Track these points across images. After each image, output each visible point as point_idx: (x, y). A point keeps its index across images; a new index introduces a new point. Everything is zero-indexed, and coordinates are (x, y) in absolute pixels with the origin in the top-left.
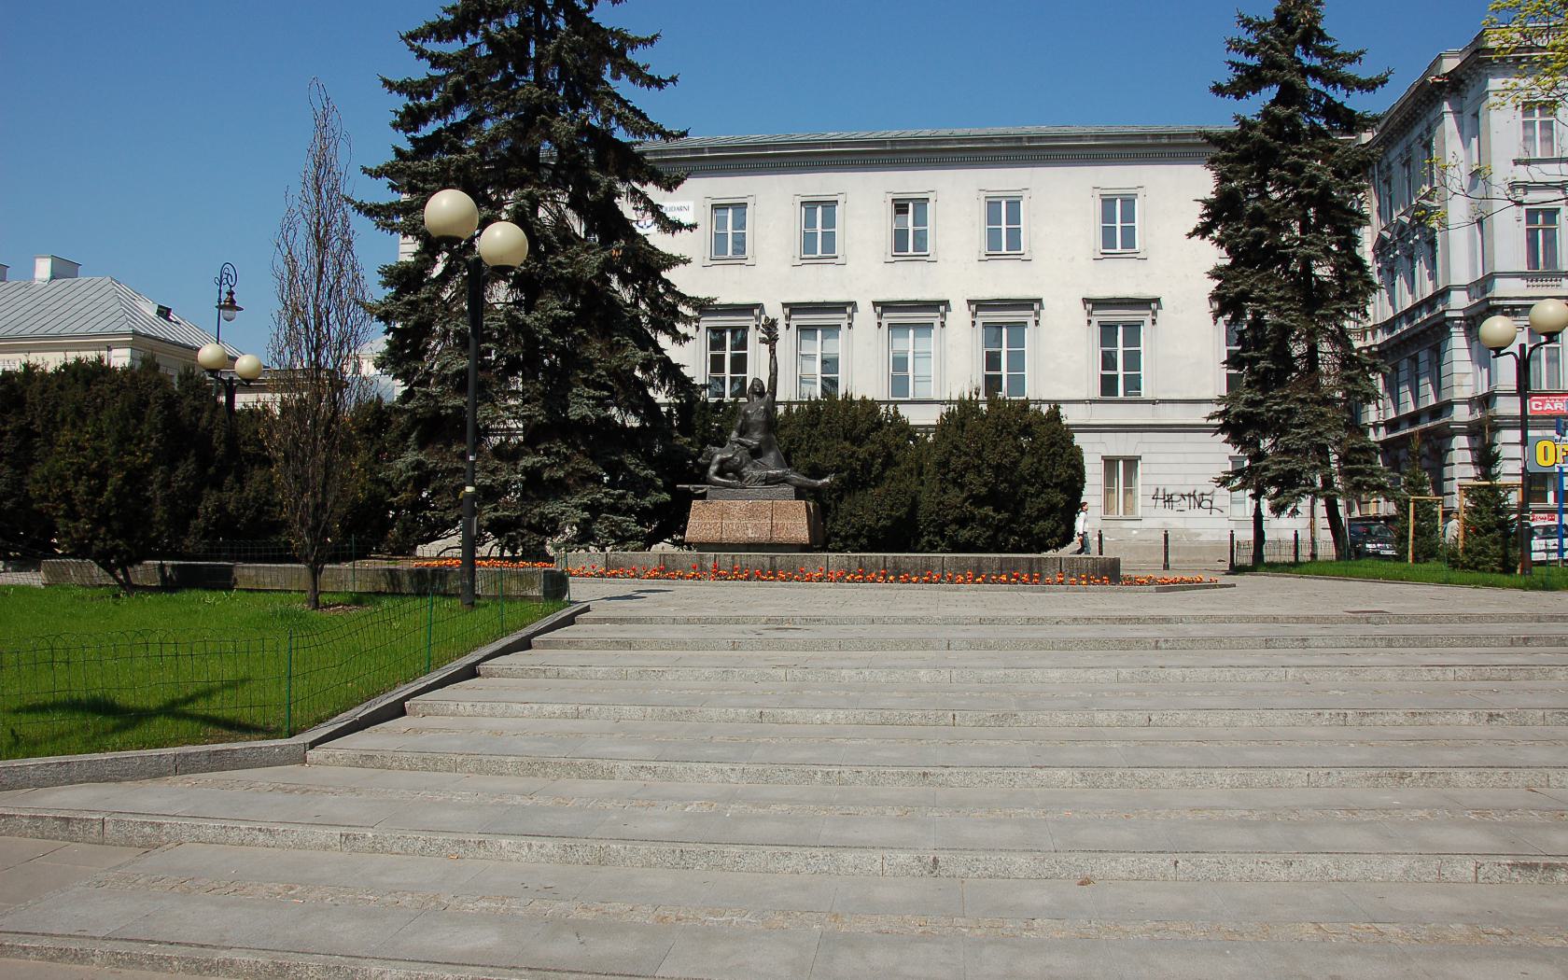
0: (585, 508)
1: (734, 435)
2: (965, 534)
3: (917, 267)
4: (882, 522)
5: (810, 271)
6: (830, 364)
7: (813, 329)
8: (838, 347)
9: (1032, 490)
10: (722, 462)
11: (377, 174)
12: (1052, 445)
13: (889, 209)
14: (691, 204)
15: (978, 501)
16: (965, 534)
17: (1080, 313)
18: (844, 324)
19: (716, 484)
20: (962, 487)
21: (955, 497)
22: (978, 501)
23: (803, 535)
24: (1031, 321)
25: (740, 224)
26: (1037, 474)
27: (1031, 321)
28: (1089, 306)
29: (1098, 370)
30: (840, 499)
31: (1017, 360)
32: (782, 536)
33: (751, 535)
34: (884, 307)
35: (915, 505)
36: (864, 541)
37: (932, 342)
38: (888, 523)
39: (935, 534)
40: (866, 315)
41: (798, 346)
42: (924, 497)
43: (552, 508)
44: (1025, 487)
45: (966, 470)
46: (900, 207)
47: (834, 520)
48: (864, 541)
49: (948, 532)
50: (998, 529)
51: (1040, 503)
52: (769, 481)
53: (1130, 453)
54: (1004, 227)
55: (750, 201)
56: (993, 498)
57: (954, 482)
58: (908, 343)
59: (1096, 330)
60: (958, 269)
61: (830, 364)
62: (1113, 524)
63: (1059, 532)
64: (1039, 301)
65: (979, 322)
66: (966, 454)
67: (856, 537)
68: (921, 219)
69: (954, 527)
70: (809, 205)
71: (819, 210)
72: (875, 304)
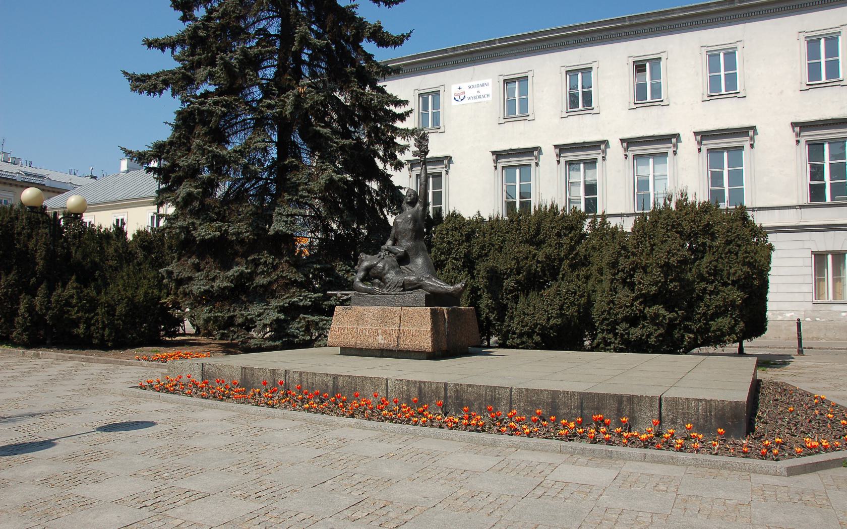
0: (282, 310)
1: (389, 243)
2: (636, 333)
3: (654, 110)
4: (552, 322)
5: (574, 120)
6: (591, 189)
7: (578, 162)
8: (597, 175)
9: (710, 288)
10: (368, 269)
11: (161, 45)
12: (728, 243)
13: (630, 69)
14: (490, 81)
15: (649, 300)
16: (636, 333)
17: (789, 135)
18: (600, 157)
19: (359, 290)
20: (632, 286)
21: (624, 295)
22: (649, 300)
23: (426, 343)
24: (747, 145)
25: (524, 91)
26: (716, 272)
27: (747, 145)
28: (797, 129)
29: (806, 181)
30: (516, 299)
31: (737, 177)
32: (407, 344)
33: (381, 341)
34: (629, 143)
35: (590, 304)
36: (537, 338)
37: (668, 167)
38: (559, 321)
39: (609, 331)
40: (616, 150)
41: (567, 176)
42: (598, 297)
43: (254, 310)
44: (703, 285)
45: (634, 269)
46: (640, 67)
47: (512, 318)
48: (537, 338)
49: (620, 329)
50: (671, 326)
51: (717, 300)
52: (406, 287)
53: (838, 248)
54: (722, 73)
55: (530, 75)
56: (662, 297)
57: (624, 282)
58: (649, 169)
59: (804, 149)
60: (687, 109)
61: (591, 189)
62: (823, 307)
63: (737, 329)
64: (753, 128)
65: (704, 149)
66: (633, 254)
67: (530, 335)
68: (656, 74)
69: (624, 325)
70: (572, 73)
71: (580, 75)
72: (622, 141)
